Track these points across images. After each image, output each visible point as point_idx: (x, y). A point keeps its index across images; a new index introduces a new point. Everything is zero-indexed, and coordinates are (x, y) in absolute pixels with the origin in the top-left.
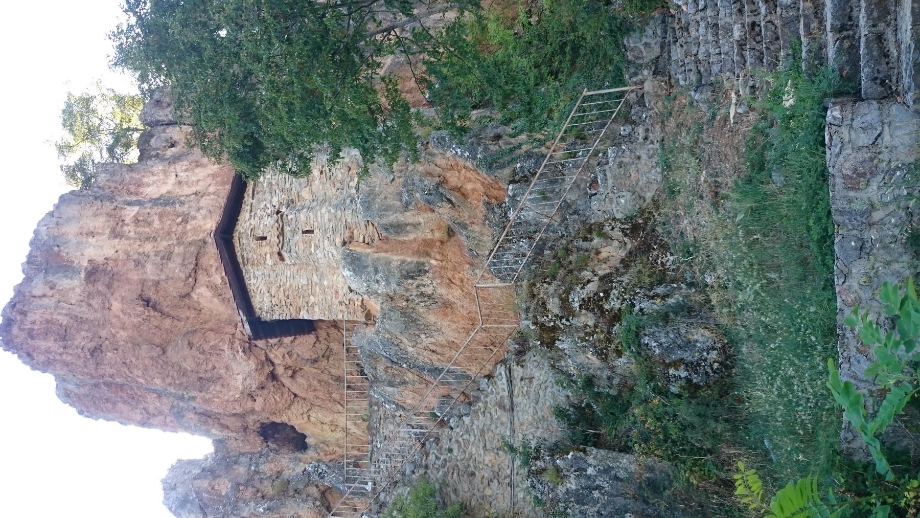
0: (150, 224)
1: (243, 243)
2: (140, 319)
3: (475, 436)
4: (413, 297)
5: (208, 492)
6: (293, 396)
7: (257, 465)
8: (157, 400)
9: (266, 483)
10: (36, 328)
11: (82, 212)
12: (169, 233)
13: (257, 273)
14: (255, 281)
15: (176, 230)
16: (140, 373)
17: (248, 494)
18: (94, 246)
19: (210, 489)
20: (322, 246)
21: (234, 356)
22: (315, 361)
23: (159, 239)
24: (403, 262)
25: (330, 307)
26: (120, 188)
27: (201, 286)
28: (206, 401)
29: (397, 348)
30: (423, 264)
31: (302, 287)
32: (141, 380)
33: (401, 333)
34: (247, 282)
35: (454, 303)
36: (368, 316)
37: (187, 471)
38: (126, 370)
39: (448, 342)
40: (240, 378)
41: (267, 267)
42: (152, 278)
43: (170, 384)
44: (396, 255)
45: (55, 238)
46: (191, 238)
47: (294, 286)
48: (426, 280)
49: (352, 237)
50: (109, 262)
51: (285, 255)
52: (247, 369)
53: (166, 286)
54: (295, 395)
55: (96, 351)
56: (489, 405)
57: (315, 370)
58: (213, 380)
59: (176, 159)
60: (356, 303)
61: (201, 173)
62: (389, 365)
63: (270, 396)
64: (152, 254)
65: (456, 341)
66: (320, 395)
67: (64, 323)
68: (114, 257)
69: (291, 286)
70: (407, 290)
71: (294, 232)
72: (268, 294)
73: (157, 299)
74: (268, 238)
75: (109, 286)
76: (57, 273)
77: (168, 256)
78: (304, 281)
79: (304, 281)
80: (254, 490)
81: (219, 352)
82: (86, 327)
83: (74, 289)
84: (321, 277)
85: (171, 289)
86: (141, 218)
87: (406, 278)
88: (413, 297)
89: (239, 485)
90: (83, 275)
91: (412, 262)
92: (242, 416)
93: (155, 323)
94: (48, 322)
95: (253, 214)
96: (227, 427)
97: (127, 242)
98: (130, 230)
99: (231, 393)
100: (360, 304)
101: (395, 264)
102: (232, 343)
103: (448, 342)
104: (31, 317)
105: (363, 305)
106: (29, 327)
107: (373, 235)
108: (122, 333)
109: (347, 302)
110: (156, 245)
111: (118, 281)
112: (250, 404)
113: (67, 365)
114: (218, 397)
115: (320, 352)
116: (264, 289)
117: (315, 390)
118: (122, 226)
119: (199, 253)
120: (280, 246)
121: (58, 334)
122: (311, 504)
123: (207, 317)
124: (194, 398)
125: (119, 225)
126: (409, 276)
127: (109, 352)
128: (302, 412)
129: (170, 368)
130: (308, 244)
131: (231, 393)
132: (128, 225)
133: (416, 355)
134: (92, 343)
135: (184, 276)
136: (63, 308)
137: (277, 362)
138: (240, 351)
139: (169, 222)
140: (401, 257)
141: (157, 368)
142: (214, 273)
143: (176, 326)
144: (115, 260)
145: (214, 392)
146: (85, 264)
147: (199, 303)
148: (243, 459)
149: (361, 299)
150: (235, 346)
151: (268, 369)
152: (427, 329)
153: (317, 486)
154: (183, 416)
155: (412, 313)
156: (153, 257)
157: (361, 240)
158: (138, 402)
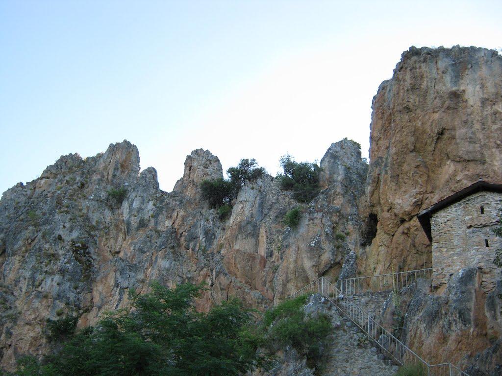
0: (494, 123)
1: (477, 200)
2: (430, 132)
3: (367, 363)
4: (448, 318)
5: (334, 193)
6: (392, 234)
7: (352, 220)
8: (385, 147)
9: (342, 227)
10: (417, 70)
11: (496, 76)
12: (488, 137)
14: (454, 211)
15: (491, 142)
16: (398, 139)
17: (335, 219)
18: (474, 91)
19: (337, 193)
20: (478, 253)
21: (413, 196)
22: (414, 246)
23: (484, 132)
24: (470, 310)
25: (440, 263)
27: (455, 166)
28: (385, 180)
29: (416, 309)
30: (470, 323)
31: (452, 242)
32: (394, 139)
33: (425, 311)
34: (453, 206)
35: (447, 344)
36: (436, 288)
37: (353, 153)
38: (399, 129)
39: (422, 341)
40: (400, 201)
41: (464, 217)
42: (457, 134)
43: (393, 158)
44: (474, 305)
45: (477, 63)
46: (486, 153)
47: (452, 237)
48: (460, 325)
49: (485, 273)
50: (464, 103)
51: (471, 230)
52: (405, 206)
53: (453, 144)
54: (393, 235)
55: (408, 109)
56: (384, 371)
57: (408, 246)
58: (398, 183)
60: (443, 279)
62: (407, 303)
63: (392, 221)
64: (473, 130)
65: (423, 346)
66: (395, 252)
67: (422, 86)
68: (468, 105)
69: (453, 235)
70: (452, 314)
71: (486, 234)
72: (446, 220)
73: (444, 139)
74: (483, 215)
75: (448, 108)
76: (454, 72)
77: (472, 141)
78: (455, 242)
79: (455, 242)
80: (337, 221)
81: (414, 185)
82: (421, 100)
83: (444, 85)
84: (459, 254)
85: (451, 147)
86: (497, 116)
87: (460, 313)
88: (448, 318)
89: (339, 212)
90: (454, 89)
91: (470, 316)
92: (379, 203)
93: (428, 141)
94: (422, 76)
95: (498, 202)
96: (372, 195)
97: (479, 111)
98: (489, 110)
99: (391, 196)
100: (443, 282)
101: (468, 305)
102: (420, 193)
103: (422, 341)
104: (423, 65)
105: (442, 284)
106: (417, 66)
107: (487, 288)
108: (420, 123)
109: (443, 273)
110: (480, 131)
112: (386, 208)
113: (398, 94)
114: (388, 188)
115: (420, 248)
116: (449, 218)
117: (397, 248)
118: (491, 104)
119: (477, 161)
120: (476, 226)
121: (415, 85)
122: (332, 258)
123: (437, 172)
124: (387, 173)
125: (491, 103)
126: (461, 315)
127: (409, 117)
128: (384, 241)
129: (402, 156)
130: (479, 244)
131: (391, 196)
132: (492, 108)
133: (413, 321)
134: (412, 106)
135: (460, 155)
136: (431, 83)
137: (412, 222)
138: (416, 200)
139: (496, 135)
140: (473, 309)
141: (402, 148)
142: (464, 173)
144: (466, 107)
145: (391, 185)
146: (462, 88)
147: (445, 165)
148: (355, 209)
149: (446, 282)
150: (419, 195)
151: (406, 218)
152: (430, 326)
153: (342, 259)
154: (376, 167)
155: (439, 317)
156: (471, 131)
157: (483, 280)
158: (384, 134)
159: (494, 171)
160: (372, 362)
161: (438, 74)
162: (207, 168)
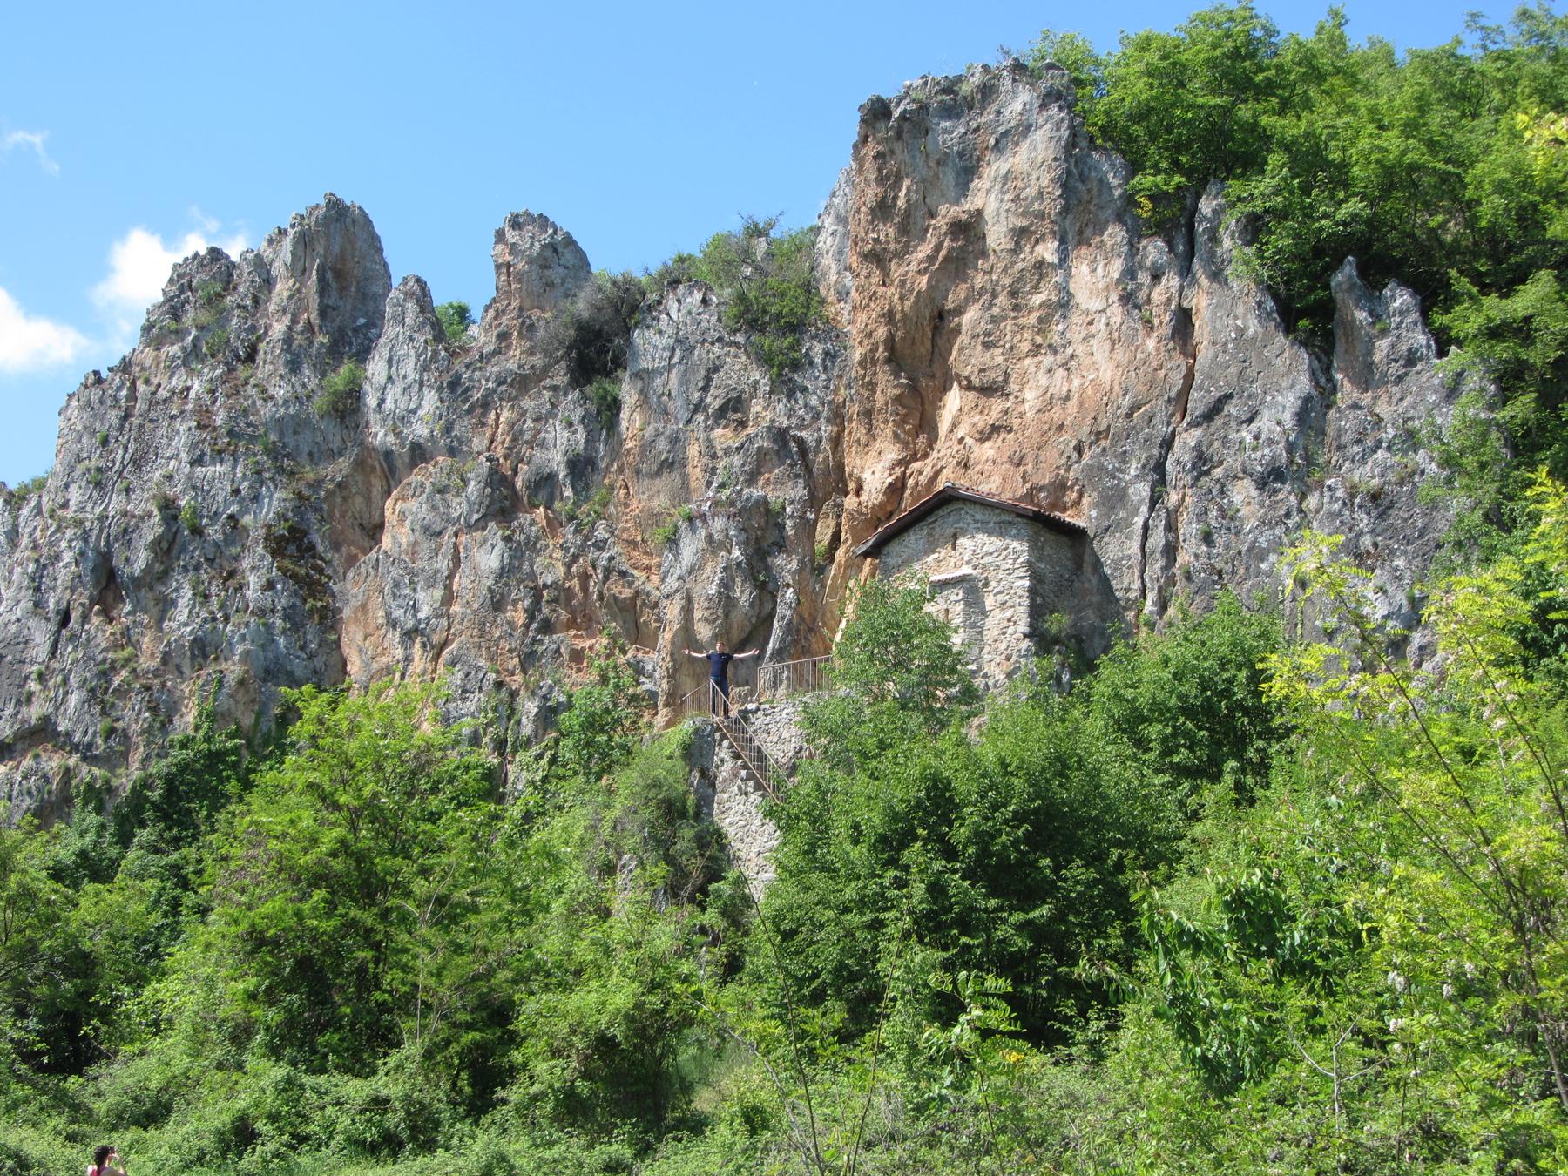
26: (1092, 208)
59: (1128, 299)
61: (1100, 348)
102: (899, 463)
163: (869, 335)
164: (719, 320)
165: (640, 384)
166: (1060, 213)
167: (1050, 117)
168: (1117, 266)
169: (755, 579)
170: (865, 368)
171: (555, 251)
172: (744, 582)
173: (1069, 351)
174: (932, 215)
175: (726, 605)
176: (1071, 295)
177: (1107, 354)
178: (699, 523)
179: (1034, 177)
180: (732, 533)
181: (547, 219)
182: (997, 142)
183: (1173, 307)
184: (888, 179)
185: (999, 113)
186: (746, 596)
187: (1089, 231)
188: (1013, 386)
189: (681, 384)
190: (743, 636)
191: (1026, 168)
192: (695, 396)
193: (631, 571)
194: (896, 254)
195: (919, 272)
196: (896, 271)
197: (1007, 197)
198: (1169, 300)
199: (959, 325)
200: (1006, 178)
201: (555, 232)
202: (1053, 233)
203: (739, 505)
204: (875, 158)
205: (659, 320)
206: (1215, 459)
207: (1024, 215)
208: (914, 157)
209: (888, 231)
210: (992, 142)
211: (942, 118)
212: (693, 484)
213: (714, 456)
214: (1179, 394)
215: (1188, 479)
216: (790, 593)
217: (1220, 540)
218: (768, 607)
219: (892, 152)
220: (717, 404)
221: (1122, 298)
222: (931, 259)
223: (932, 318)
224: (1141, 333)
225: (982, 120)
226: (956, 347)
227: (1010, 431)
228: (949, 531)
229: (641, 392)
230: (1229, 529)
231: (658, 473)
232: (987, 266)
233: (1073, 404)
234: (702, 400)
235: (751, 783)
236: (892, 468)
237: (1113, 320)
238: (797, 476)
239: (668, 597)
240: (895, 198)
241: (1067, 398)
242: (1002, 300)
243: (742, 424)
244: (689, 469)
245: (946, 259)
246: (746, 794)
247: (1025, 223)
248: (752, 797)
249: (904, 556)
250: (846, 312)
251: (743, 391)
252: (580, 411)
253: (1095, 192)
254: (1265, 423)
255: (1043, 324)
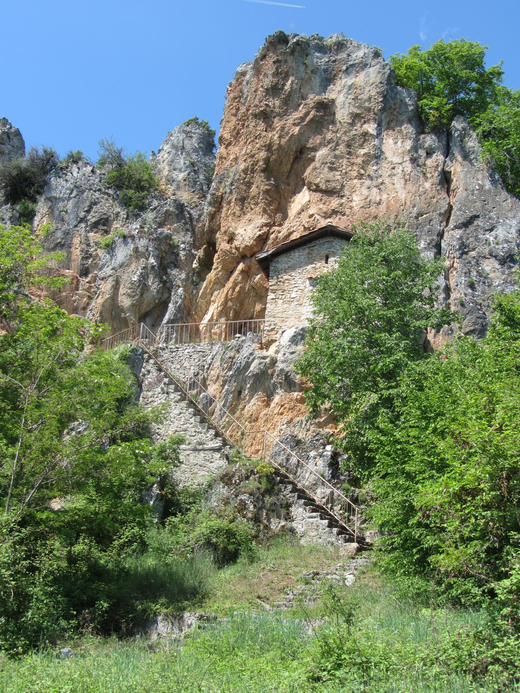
13: (303, 257)
26: (395, 113)
50: (332, 117)
52: (247, 238)
59: (414, 160)
61: (399, 183)
93: (284, 160)
102: (266, 225)
108: (277, 136)
111: (316, 127)
115: (260, 291)
138: (260, 233)
143: (283, 176)
150: (264, 228)
159: (351, 208)
160: (188, 425)
161: (306, 73)
162: (4, 144)
163: (253, 156)
164: (100, 181)
165: (50, 204)
166: (380, 110)
167: (379, 62)
168: (409, 144)
169: (161, 278)
170: (246, 174)
171: (9, 137)
172: (155, 278)
173: (380, 180)
174: (304, 98)
175: (143, 288)
176: (382, 152)
177: (402, 185)
178: (129, 240)
179: (367, 89)
180: (150, 249)
181: (7, 120)
182: (347, 69)
183: (439, 169)
184: (281, 74)
185: (349, 55)
186: (155, 286)
187: (393, 124)
188: (346, 192)
189: (74, 207)
190: (148, 309)
191: (362, 84)
192: (82, 214)
193: (30, 295)
194: (279, 115)
195: (294, 124)
196: (278, 123)
197: (350, 97)
198: (438, 166)
199: (314, 156)
200: (350, 87)
201: (11, 128)
202: (375, 119)
203: (155, 236)
204: (274, 62)
205: (66, 175)
206: (471, 246)
207: (359, 107)
208: (298, 66)
209: (276, 103)
210: (344, 68)
211: (316, 51)
212: (74, 257)
213: (88, 245)
214: (445, 212)
215: (457, 254)
216: (180, 290)
217: (479, 288)
218: (166, 296)
219: (286, 61)
220: (93, 220)
221: (411, 159)
222: (303, 119)
223: (297, 151)
224: (422, 179)
225: (339, 57)
226: (311, 167)
227: (343, 215)
228: (324, 252)
229: (50, 208)
230: (484, 283)
231: (54, 249)
232: (334, 129)
233: (383, 207)
234: (85, 217)
235: (173, 386)
236: (262, 227)
237: (406, 169)
238: (187, 230)
239: (103, 279)
240: (284, 85)
241: (379, 203)
242: (342, 148)
243: (107, 232)
244: (73, 249)
245: (311, 121)
246: (168, 393)
247: (358, 112)
248: (172, 396)
249: (290, 264)
250: (171, 190)
251: (110, 216)
252: (9, 215)
253: (398, 106)
254: (500, 232)
255: (365, 164)
